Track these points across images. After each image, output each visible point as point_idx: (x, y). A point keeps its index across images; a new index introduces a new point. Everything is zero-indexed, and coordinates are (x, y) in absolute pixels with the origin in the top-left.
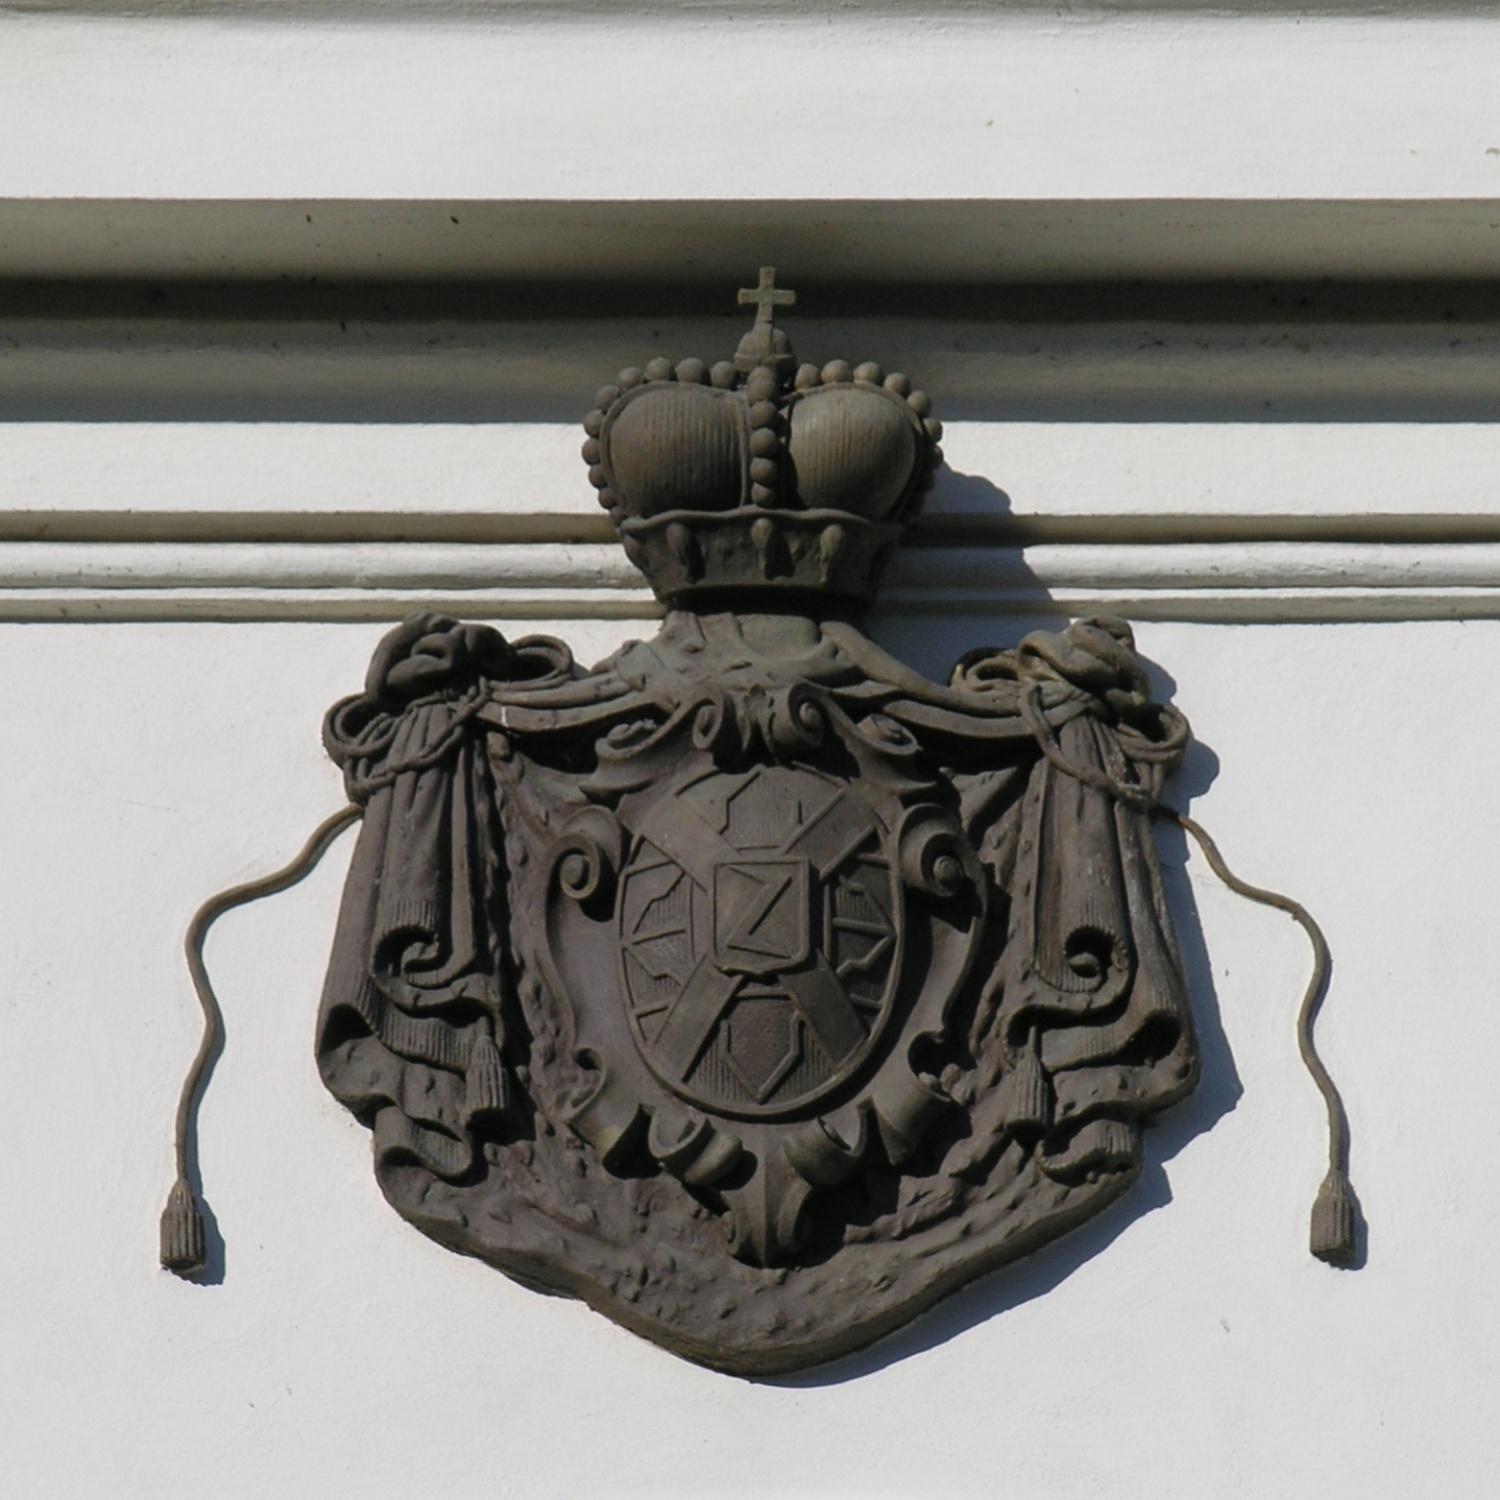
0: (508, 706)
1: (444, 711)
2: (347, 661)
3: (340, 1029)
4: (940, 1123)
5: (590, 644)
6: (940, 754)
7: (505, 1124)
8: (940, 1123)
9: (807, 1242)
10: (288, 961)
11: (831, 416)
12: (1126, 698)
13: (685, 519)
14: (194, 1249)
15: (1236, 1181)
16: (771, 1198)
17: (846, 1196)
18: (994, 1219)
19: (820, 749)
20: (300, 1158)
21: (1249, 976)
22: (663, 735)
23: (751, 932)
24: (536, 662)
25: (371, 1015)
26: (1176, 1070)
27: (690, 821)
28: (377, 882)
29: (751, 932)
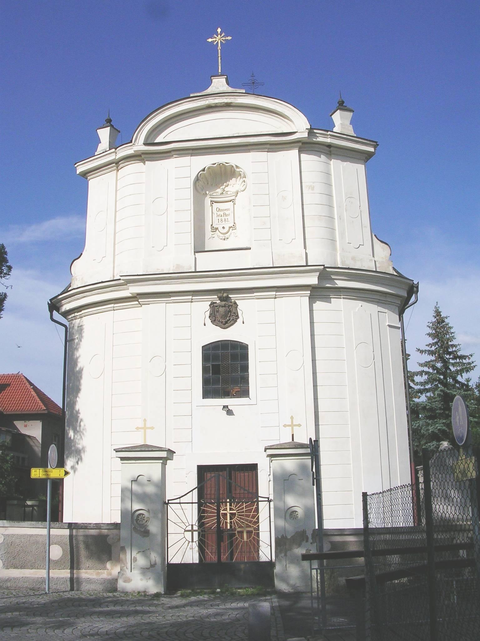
0: (215, 305)
1: (212, 305)
2: (209, 303)
3: (209, 317)
4: (230, 319)
5: (218, 302)
6: (229, 306)
7: (215, 320)
8: (230, 319)
9: (225, 324)
10: (208, 314)
11: (225, 295)
12: (235, 303)
13: (221, 299)
14: (205, 325)
15: (239, 321)
16: (224, 323)
17: (226, 322)
18: (231, 323)
19: (225, 307)
20: (208, 321)
21: (240, 313)
22: (220, 306)
23: (293, 435)
24: (216, 303)
25: (286, 603)
26: (237, 317)
27: (221, 309)
28: (218, 334)
29: (293, 435)
